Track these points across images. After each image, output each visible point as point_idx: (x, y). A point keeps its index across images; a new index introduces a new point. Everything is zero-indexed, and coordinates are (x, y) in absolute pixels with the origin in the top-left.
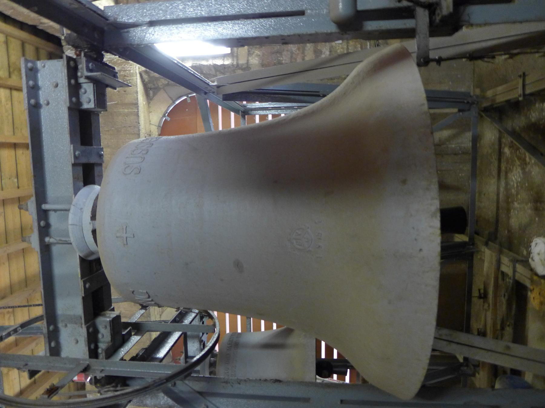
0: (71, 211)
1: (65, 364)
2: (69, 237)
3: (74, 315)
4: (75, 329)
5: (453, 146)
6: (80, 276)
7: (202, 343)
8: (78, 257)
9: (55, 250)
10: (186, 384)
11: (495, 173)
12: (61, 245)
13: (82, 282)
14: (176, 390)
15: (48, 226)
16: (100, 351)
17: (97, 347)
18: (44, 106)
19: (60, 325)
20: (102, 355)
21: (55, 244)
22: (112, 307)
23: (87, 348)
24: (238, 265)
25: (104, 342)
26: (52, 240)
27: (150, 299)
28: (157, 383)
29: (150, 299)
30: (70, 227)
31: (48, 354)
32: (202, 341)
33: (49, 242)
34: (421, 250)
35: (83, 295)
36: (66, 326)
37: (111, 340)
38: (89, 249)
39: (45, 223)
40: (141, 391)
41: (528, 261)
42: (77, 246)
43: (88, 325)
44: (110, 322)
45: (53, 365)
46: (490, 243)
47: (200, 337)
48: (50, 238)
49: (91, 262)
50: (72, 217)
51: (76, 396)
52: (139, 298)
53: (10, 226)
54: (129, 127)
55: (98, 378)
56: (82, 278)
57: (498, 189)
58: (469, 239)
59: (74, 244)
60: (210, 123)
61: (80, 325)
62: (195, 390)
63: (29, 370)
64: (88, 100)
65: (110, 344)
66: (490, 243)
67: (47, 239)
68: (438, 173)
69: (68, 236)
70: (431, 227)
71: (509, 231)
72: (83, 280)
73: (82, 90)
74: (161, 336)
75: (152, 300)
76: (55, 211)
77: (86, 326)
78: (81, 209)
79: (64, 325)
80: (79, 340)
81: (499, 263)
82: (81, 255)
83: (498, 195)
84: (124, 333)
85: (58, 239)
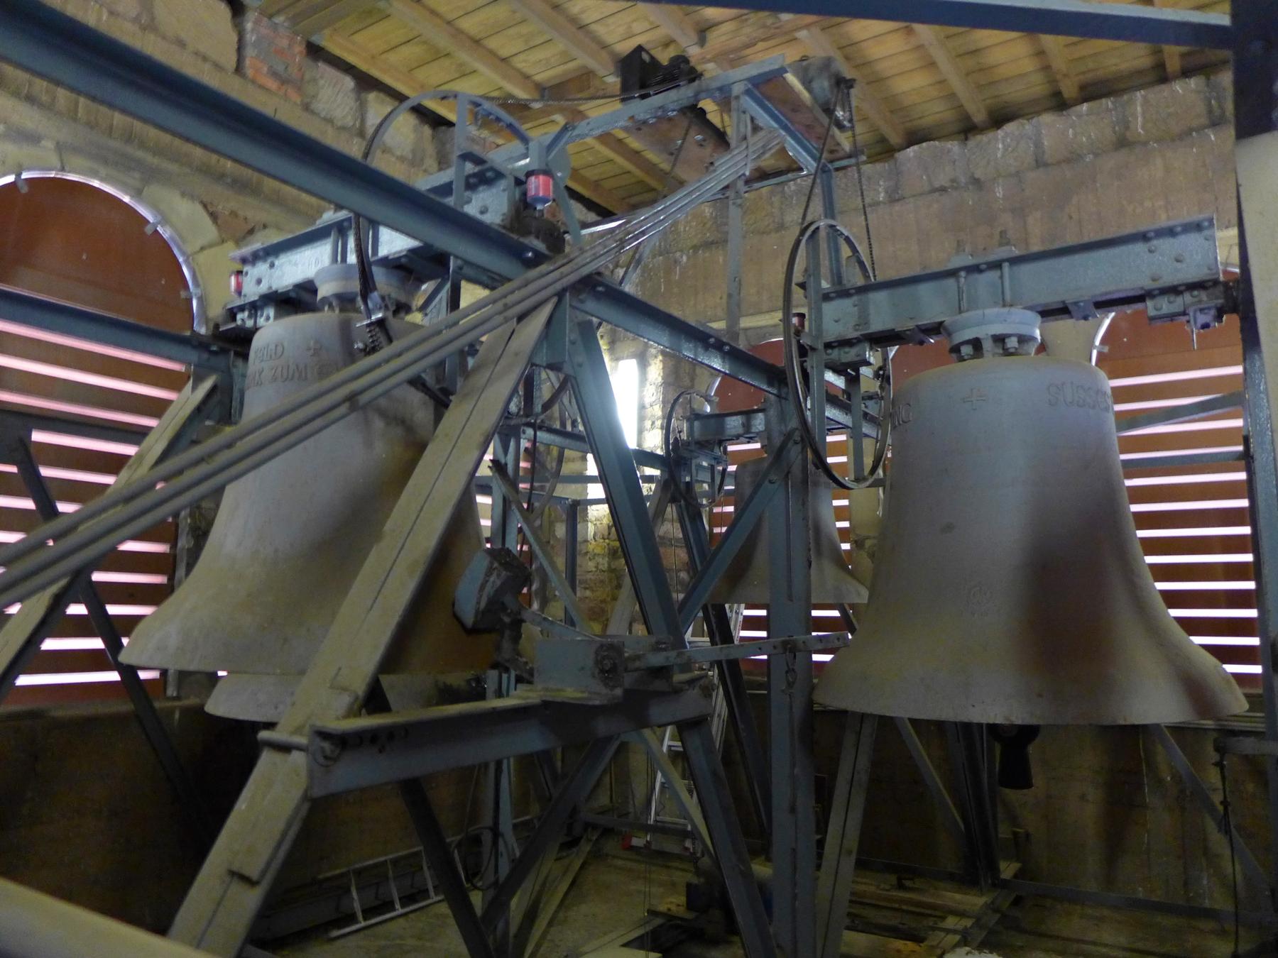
0: (999, 329)
5: (1205, 882)
6: (920, 323)
8: (943, 319)
9: (951, 282)
10: (797, 457)
11: (1140, 945)
14: (790, 444)
18: (1147, 245)
19: (855, 298)
21: (958, 282)
24: (949, 528)
25: (840, 354)
26: (962, 280)
27: (901, 422)
29: (901, 422)
34: (973, 706)
36: (855, 306)
41: (966, 945)
46: (998, 916)
50: (992, 312)
51: (677, 180)
54: (1217, 208)
55: (805, 364)
56: (917, 326)
57: (1106, 945)
58: (1005, 880)
59: (959, 317)
60: (1197, 413)
63: (805, 282)
64: (1159, 306)
66: (998, 916)
67: (963, 274)
68: (583, 75)
70: (996, 715)
71: (1021, 948)
73: (1172, 298)
75: (900, 424)
76: (1001, 277)
78: (1005, 321)
79: (856, 303)
81: (961, 914)
83: (1094, 943)
85: (964, 289)
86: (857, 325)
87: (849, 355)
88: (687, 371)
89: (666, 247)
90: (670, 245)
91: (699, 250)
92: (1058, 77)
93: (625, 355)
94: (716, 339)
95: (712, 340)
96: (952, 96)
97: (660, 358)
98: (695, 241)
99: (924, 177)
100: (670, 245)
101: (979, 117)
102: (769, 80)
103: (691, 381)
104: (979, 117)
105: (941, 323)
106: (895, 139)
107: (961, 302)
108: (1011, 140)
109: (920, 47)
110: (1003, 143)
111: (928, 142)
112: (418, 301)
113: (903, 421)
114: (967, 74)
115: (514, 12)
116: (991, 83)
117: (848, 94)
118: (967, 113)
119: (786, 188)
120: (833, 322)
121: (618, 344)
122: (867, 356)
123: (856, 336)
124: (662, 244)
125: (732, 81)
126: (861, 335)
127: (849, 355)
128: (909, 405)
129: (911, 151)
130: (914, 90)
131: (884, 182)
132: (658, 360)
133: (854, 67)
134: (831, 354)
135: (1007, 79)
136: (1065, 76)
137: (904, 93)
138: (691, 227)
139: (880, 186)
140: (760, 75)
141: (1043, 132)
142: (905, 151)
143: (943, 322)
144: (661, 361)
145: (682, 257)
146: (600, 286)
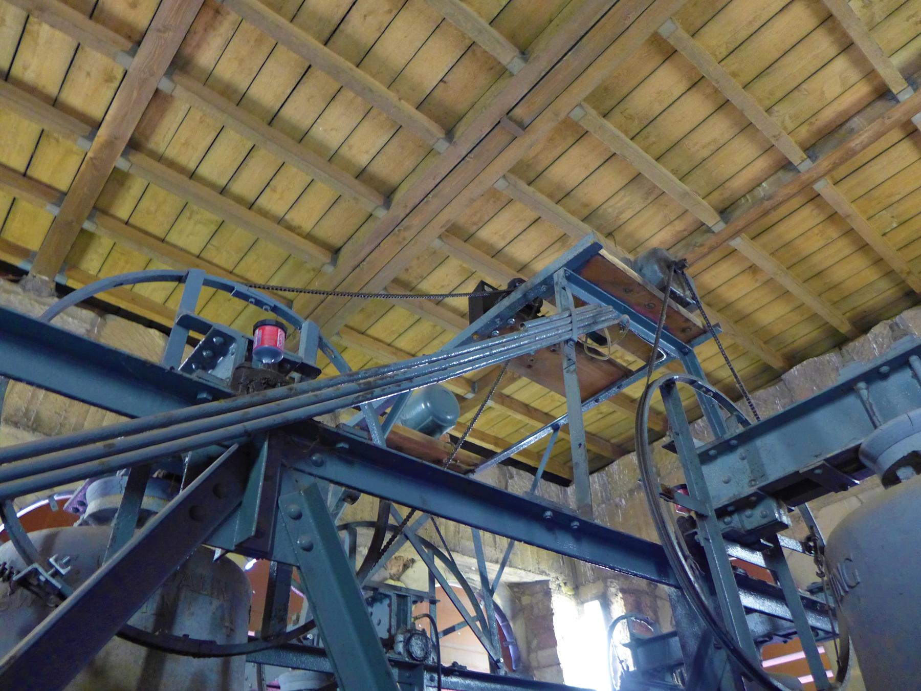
1: (697, 484)
2: (885, 422)
3: (763, 465)
4: (744, 473)
6: (828, 456)
7: (767, 639)
8: (857, 443)
9: (850, 401)
10: (725, 668)
12: (862, 407)
13: (822, 462)
14: (711, 650)
15: (884, 377)
16: (727, 519)
17: (730, 514)
19: (741, 451)
20: (722, 526)
22: (793, 508)
23: (726, 503)
25: (741, 521)
26: (864, 393)
27: (847, 589)
28: (726, 637)
29: (847, 589)
30: (903, 418)
31: (698, 452)
32: (771, 639)
33: (859, 389)
35: (801, 472)
36: (743, 459)
37: (748, 531)
38: (880, 455)
39: (886, 372)
40: (708, 618)
42: (877, 436)
43: (759, 492)
44: (774, 521)
45: (689, 468)
47: (776, 633)
48: (867, 389)
49: (857, 459)
52: (842, 570)
53: (816, 259)
55: (696, 537)
56: (827, 460)
59: (877, 432)
61: (752, 478)
62: (720, 682)
63: (673, 441)
65: (743, 531)
67: (862, 385)
69: (887, 418)
72: (825, 463)
74: (771, 590)
75: (846, 592)
77: (758, 491)
80: (730, 483)
82: (863, 446)
84: (762, 541)
85: (871, 401)
86: (753, 480)
87: (753, 519)
88: (649, 605)
89: (606, 495)
90: (610, 494)
91: (634, 492)
92: (903, 276)
93: (589, 598)
94: (552, 510)
95: (576, 524)
96: (814, 317)
97: (620, 595)
98: (630, 486)
99: (815, 388)
100: (610, 494)
101: (845, 328)
102: (588, 262)
103: (655, 615)
104: (845, 328)
105: (857, 449)
106: (777, 364)
107: (874, 418)
108: (883, 339)
109: (769, 282)
110: (876, 343)
111: (808, 360)
112: (391, 569)
113: (850, 587)
114: (820, 295)
115: (434, 326)
116: (844, 299)
117: (683, 273)
118: (831, 326)
119: (696, 426)
120: (724, 485)
121: (582, 589)
122: (777, 515)
123: (753, 492)
124: (604, 494)
125: (553, 271)
126: (758, 489)
127: (753, 519)
128: (851, 561)
129: (794, 371)
130: (778, 318)
131: (780, 400)
132: (619, 597)
133: (718, 311)
134: (730, 523)
135: (857, 292)
136: (909, 273)
137: (770, 323)
138: (624, 474)
139: (777, 404)
140: (576, 258)
141: (910, 325)
142: (790, 371)
143: (859, 446)
144: (621, 598)
145: (621, 501)
146: (340, 441)
